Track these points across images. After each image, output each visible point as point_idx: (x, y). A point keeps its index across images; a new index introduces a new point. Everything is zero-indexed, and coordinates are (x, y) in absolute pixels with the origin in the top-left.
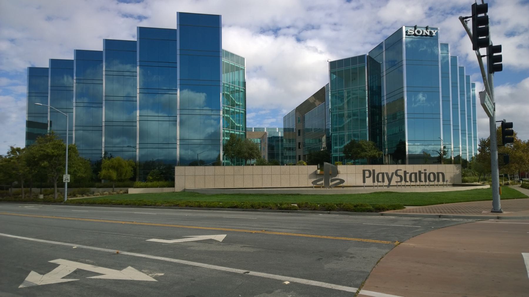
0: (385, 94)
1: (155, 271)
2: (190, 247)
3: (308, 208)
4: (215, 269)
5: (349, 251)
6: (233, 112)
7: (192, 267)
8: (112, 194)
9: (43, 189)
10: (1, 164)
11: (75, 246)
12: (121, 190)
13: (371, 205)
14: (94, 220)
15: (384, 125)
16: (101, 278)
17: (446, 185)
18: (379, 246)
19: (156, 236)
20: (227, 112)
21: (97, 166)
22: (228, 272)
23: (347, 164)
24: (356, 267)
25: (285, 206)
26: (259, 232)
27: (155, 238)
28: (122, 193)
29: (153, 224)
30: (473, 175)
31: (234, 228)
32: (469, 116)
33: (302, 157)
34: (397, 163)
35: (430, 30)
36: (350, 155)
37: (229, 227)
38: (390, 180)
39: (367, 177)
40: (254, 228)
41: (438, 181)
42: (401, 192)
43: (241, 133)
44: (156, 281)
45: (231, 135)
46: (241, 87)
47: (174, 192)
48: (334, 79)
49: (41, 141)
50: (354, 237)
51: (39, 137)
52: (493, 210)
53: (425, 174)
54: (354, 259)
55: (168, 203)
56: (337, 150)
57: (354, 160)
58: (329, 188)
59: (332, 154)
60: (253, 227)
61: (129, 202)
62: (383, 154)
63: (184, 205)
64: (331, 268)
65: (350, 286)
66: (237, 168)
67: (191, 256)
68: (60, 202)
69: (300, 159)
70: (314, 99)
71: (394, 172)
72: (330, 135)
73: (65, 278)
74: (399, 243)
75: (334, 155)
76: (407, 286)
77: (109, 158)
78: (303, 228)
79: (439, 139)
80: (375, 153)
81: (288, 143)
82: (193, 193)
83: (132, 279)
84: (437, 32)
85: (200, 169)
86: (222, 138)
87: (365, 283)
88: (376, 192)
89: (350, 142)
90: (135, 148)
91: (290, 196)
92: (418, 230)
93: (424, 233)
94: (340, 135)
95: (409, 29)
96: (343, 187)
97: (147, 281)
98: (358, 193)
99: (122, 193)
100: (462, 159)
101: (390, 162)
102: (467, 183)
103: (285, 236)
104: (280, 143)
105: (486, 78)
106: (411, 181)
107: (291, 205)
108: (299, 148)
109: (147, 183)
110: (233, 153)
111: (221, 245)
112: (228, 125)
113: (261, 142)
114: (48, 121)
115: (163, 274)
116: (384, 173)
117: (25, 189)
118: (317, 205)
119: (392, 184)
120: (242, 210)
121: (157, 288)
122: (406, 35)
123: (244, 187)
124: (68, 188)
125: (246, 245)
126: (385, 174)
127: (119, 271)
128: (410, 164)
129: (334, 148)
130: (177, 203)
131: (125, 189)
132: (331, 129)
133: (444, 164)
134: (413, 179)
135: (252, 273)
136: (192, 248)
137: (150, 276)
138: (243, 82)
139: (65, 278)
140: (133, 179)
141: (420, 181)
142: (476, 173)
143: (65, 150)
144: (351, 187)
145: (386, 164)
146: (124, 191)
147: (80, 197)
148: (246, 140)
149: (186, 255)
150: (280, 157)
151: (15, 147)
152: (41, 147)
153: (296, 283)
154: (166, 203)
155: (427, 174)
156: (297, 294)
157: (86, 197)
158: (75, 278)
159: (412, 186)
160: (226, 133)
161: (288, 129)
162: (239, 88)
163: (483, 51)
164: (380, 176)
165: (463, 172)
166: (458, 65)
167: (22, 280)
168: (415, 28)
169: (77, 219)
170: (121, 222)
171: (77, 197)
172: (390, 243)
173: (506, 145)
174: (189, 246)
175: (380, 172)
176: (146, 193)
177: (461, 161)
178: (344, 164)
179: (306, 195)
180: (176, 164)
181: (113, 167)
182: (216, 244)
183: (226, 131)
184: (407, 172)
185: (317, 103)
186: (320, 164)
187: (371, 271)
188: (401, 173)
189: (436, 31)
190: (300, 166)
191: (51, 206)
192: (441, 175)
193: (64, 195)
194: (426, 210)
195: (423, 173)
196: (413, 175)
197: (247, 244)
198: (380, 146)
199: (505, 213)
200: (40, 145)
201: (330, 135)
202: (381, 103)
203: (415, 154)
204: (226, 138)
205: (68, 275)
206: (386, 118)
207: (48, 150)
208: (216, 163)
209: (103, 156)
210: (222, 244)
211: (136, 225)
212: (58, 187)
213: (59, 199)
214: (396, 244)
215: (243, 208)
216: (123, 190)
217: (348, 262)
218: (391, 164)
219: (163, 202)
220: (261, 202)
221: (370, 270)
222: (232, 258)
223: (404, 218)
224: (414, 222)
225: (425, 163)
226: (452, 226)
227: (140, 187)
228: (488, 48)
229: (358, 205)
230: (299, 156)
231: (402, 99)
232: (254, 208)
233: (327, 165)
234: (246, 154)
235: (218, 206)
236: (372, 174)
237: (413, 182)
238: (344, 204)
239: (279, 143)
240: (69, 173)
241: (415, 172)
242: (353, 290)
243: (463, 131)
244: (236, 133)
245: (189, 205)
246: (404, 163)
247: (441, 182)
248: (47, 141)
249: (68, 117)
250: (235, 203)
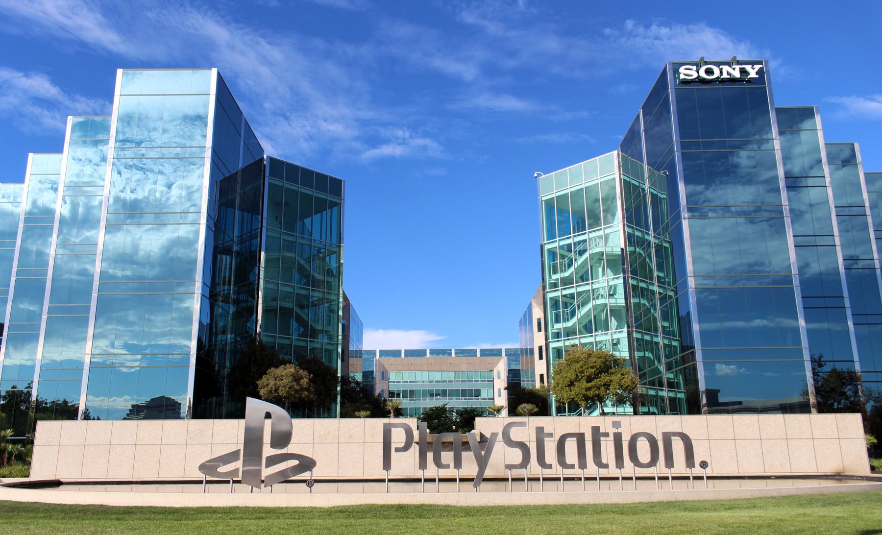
39: (397, 450)
41: (669, 462)
53: (618, 438)
84: (761, 69)
96: (310, 483)
189: (757, 67)
247: (470, 468)
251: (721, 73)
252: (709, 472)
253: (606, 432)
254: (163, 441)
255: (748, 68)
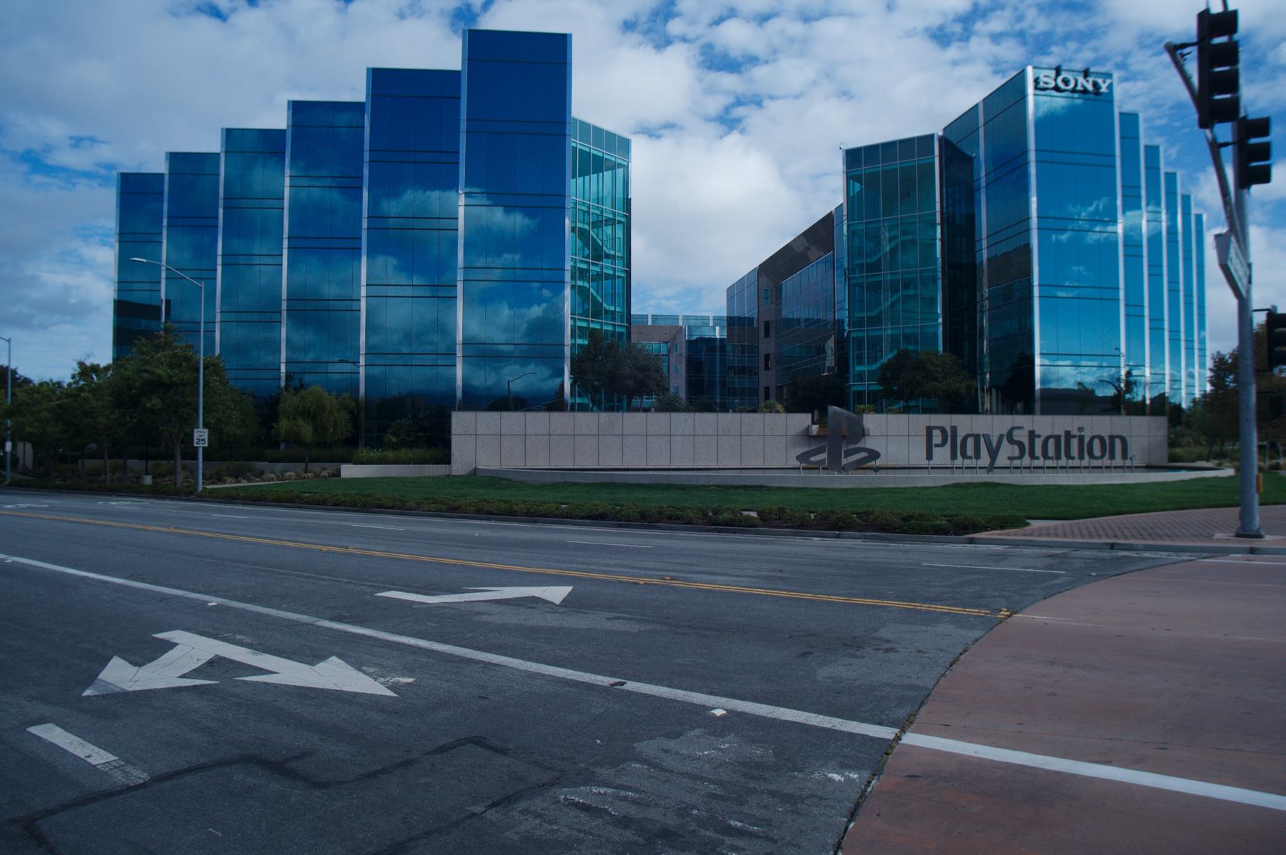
0: (984, 234)
1: (395, 671)
2: (482, 616)
3: (785, 522)
4: (539, 671)
5: (884, 633)
6: (597, 275)
7: (482, 665)
8: (304, 478)
9: (151, 463)
10: (1282, 461)
11: (213, 601)
12: (324, 469)
13: (945, 516)
14: (259, 540)
15: (982, 312)
16: (269, 681)
17: (1130, 467)
18: (958, 621)
19: (399, 586)
20: (583, 274)
21: (268, 408)
22: (571, 680)
23: (887, 412)
24: (899, 676)
25: (727, 516)
26: (655, 581)
27: (396, 590)
28: (326, 474)
29: (393, 555)
30: (1195, 445)
31: (592, 571)
32: (1188, 295)
33: (773, 392)
34: (1011, 411)
36: (896, 388)
37: (580, 566)
38: (993, 454)
39: (937, 446)
40: (643, 572)
41: (1112, 457)
43: (618, 329)
44: (396, 695)
45: (593, 335)
46: (619, 211)
47: (449, 476)
48: (856, 192)
49: (145, 349)
50: (898, 598)
51: (139, 340)
52: (1240, 530)
53: (1081, 439)
54: (894, 654)
55: (433, 503)
56: (863, 374)
57: (907, 401)
58: (841, 472)
59: (851, 385)
60: (640, 569)
61: (342, 499)
62: (979, 387)
63: (473, 508)
64: (833, 678)
65: (880, 724)
66: (605, 417)
67: (482, 637)
68: (188, 494)
69: (767, 397)
70: (806, 244)
71: (1005, 432)
72: (846, 335)
73: (187, 676)
74: (1008, 613)
75: (855, 386)
76: (1020, 724)
77: (297, 390)
78: (768, 573)
79: (1116, 353)
80: (958, 384)
81: (738, 356)
82: (494, 480)
83: (338, 689)
85: (513, 420)
86: (568, 340)
87: (917, 717)
88: (959, 484)
89: (895, 356)
90: (357, 364)
91: (741, 491)
92: (1058, 581)
93: (1072, 588)
94: (872, 336)
95: (1042, 74)
96: (877, 469)
97: (372, 694)
98: (914, 485)
99: (326, 474)
100: (1170, 403)
101: (994, 409)
102: (1180, 464)
103: (721, 592)
104: (718, 354)
105: (1230, 199)
106: (1046, 456)
107: (742, 514)
108: (767, 368)
109: (385, 453)
110: (596, 380)
111: (557, 613)
112: (586, 307)
113: (669, 351)
114: (162, 300)
115: (411, 680)
116: (979, 435)
117: (111, 461)
118: (807, 514)
119: (999, 462)
120: (616, 524)
121: (397, 713)
122: (1036, 88)
123: (623, 467)
124: (204, 460)
125: (622, 615)
126: (982, 439)
127: (309, 666)
128: (1043, 413)
129: (854, 369)
130: (456, 504)
131: (335, 465)
132: (847, 320)
133: (1128, 414)
134: (1051, 452)
135: (631, 686)
136: (484, 616)
137: (382, 684)
138: (624, 198)
139: (187, 676)
140: (352, 442)
141: (1069, 456)
142: (1203, 439)
143: (198, 370)
144: (897, 470)
145: (985, 412)
146: (330, 471)
147: (231, 483)
148: (630, 347)
149: (471, 635)
150: (718, 391)
151: (88, 363)
152: (146, 363)
153: (743, 713)
154: (429, 504)
155: (1087, 440)
156: (744, 742)
157: (244, 483)
158: (209, 677)
159: (1048, 468)
160: (579, 327)
161: (739, 318)
162: (614, 214)
163: (1224, 131)
164: (970, 442)
165: (1172, 436)
166: (1163, 169)
167: (91, 678)
168: (1058, 71)
169: (220, 536)
170: (319, 547)
171: (225, 482)
172: (986, 614)
173: (1276, 370)
174: (478, 614)
175: (970, 433)
176: (382, 478)
177: (1167, 407)
178: (878, 410)
179: (780, 488)
180: (455, 407)
181: (305, 413)
182: (546, 610)
183: (579, 324)
184: (1036, 433)
185: (813, 252)
186: (819, 412)
187: (935, 686)
188: (1021, 436)
189: (1108, 81)
190: (768, 416)
191: (167, 502)
192: (1118, 442)
193: (196, 479)
194: (1080, 531)
195: (1075, 437)
196: (1051, 442)
197: (624, 612)
198: (972, 368)
199: (1269, 540)
200: (142, 357)
201: (846, 335)
202: (974, 255)
203: (1057, 390)
204: (579, 341)
205: (195, 670)
206: (987, 295)
207: (159, 371)
208: (554, 403)
209: (283, 383)
210: (561, 610)
211: (354, 555)
212: (184, 457)
213: (187, 486)
214: (1002, 616)
215: (620, 521)
216: (329, 468)
217: (878, 661)
218: (997, 413)
219: (422, 501)
220: (664, 505)
221: (933, 682)
222: (582, 647)
223: (1024, 550)
224: (1049, 561)
225: (1082, 412)
226: (1140, 570)
227: (368, 463)
228: (1235, 123)
229: (911, 516)
230: (767, 389)
231: (1027, 249)
232: (649, 520)
233: (835, 412)
234: (630, 383)
235: (557, 512)
236: (949, 438)
237: (1051, 458)
238: (876, 514)
239: (715, 355)
240: (205, 426)
241: (1056, 433)
242: (886, 733)
243: (1174, 332)
244: (605, 328)
245: (486, 509)
246: (1029, 410)
247: (1118, 461)
248: (158, 348)
249: (203, 290)
250: (598, 507)
253: (1027, 435)
254: (696, 431)
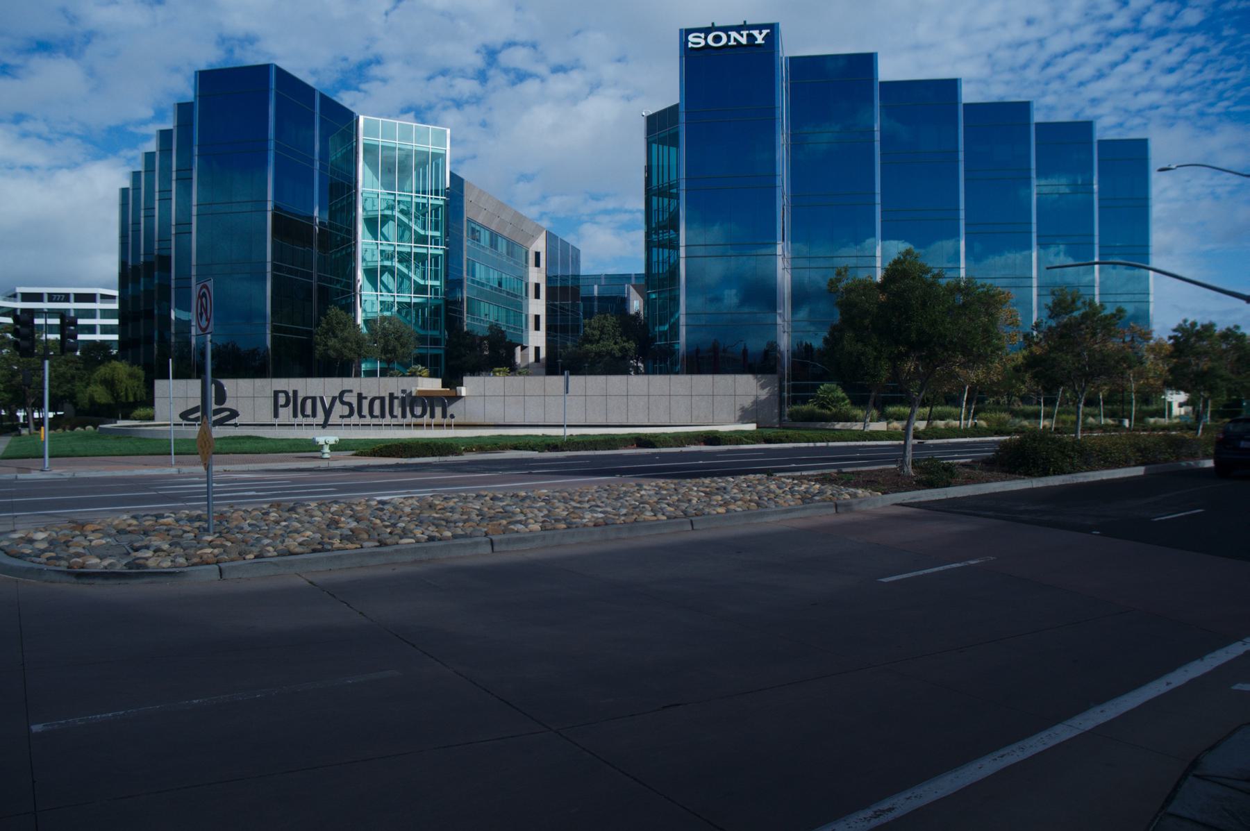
35: (747, 32)
38: (328, 413)
39: (282, 406)
41: (432, 416)
42: (280, 438)
71: (337, 395)
96: (236, 425)
134: (377, 411)
184: (364, 395)
189: (765, 32)
195: (397, 398)
241: (382, 395)
247: (438, 418)
251: (729, 40)
252: (453, 421)
255: (756, 33)
